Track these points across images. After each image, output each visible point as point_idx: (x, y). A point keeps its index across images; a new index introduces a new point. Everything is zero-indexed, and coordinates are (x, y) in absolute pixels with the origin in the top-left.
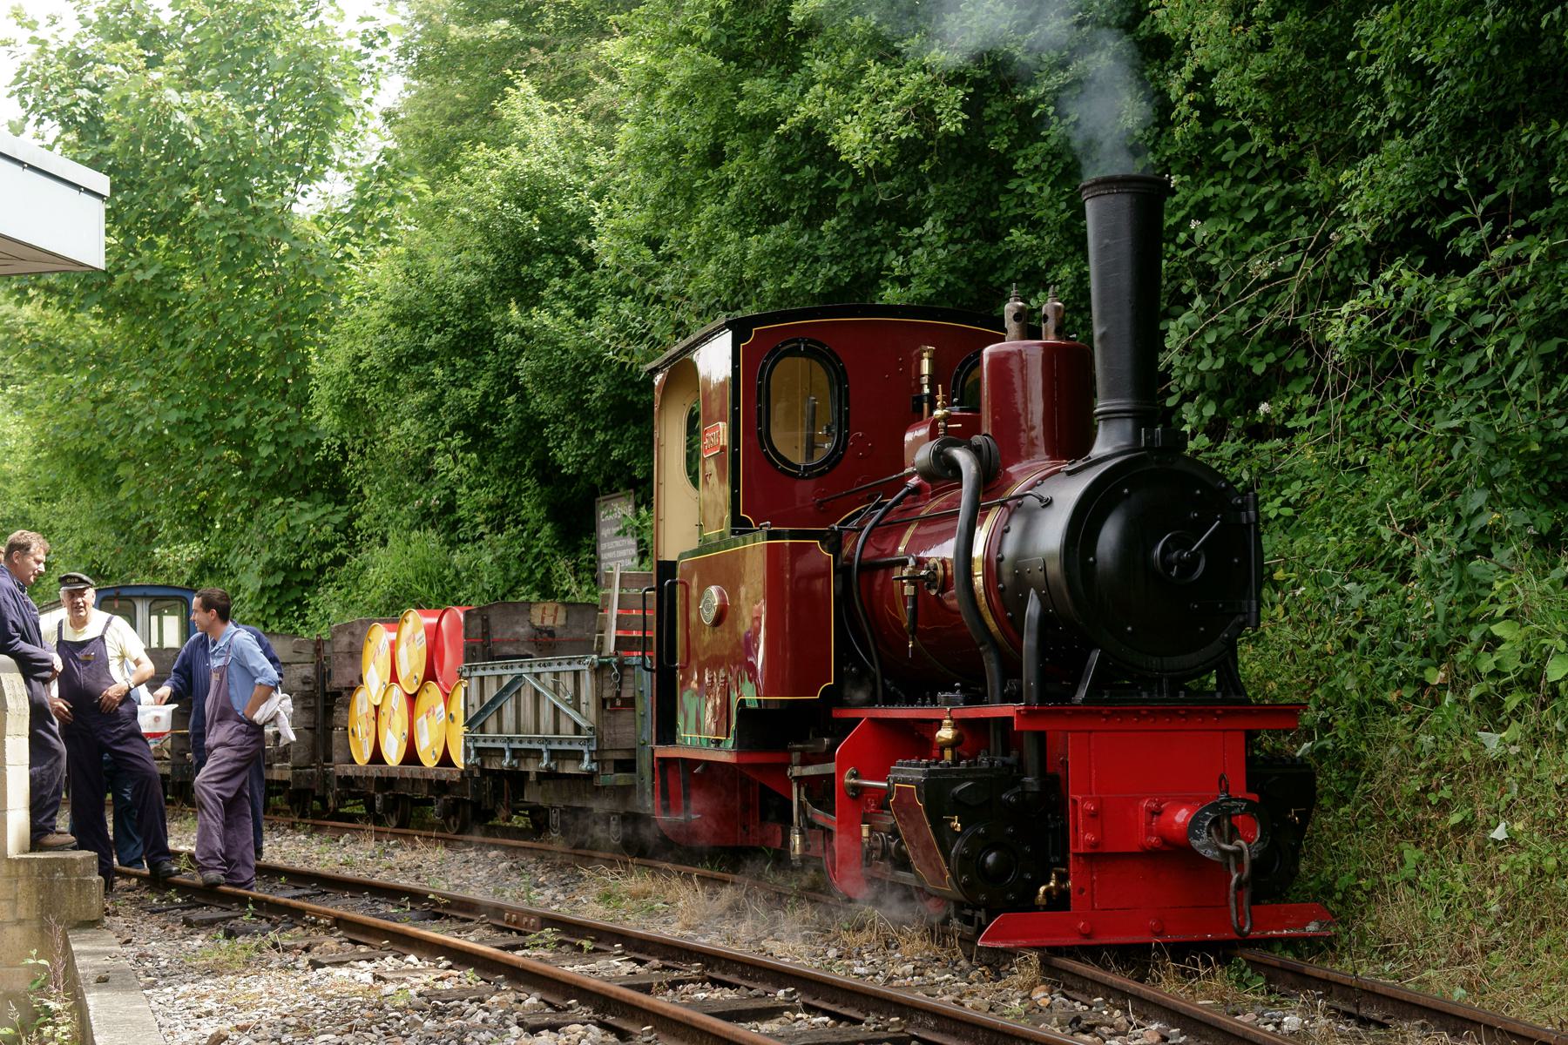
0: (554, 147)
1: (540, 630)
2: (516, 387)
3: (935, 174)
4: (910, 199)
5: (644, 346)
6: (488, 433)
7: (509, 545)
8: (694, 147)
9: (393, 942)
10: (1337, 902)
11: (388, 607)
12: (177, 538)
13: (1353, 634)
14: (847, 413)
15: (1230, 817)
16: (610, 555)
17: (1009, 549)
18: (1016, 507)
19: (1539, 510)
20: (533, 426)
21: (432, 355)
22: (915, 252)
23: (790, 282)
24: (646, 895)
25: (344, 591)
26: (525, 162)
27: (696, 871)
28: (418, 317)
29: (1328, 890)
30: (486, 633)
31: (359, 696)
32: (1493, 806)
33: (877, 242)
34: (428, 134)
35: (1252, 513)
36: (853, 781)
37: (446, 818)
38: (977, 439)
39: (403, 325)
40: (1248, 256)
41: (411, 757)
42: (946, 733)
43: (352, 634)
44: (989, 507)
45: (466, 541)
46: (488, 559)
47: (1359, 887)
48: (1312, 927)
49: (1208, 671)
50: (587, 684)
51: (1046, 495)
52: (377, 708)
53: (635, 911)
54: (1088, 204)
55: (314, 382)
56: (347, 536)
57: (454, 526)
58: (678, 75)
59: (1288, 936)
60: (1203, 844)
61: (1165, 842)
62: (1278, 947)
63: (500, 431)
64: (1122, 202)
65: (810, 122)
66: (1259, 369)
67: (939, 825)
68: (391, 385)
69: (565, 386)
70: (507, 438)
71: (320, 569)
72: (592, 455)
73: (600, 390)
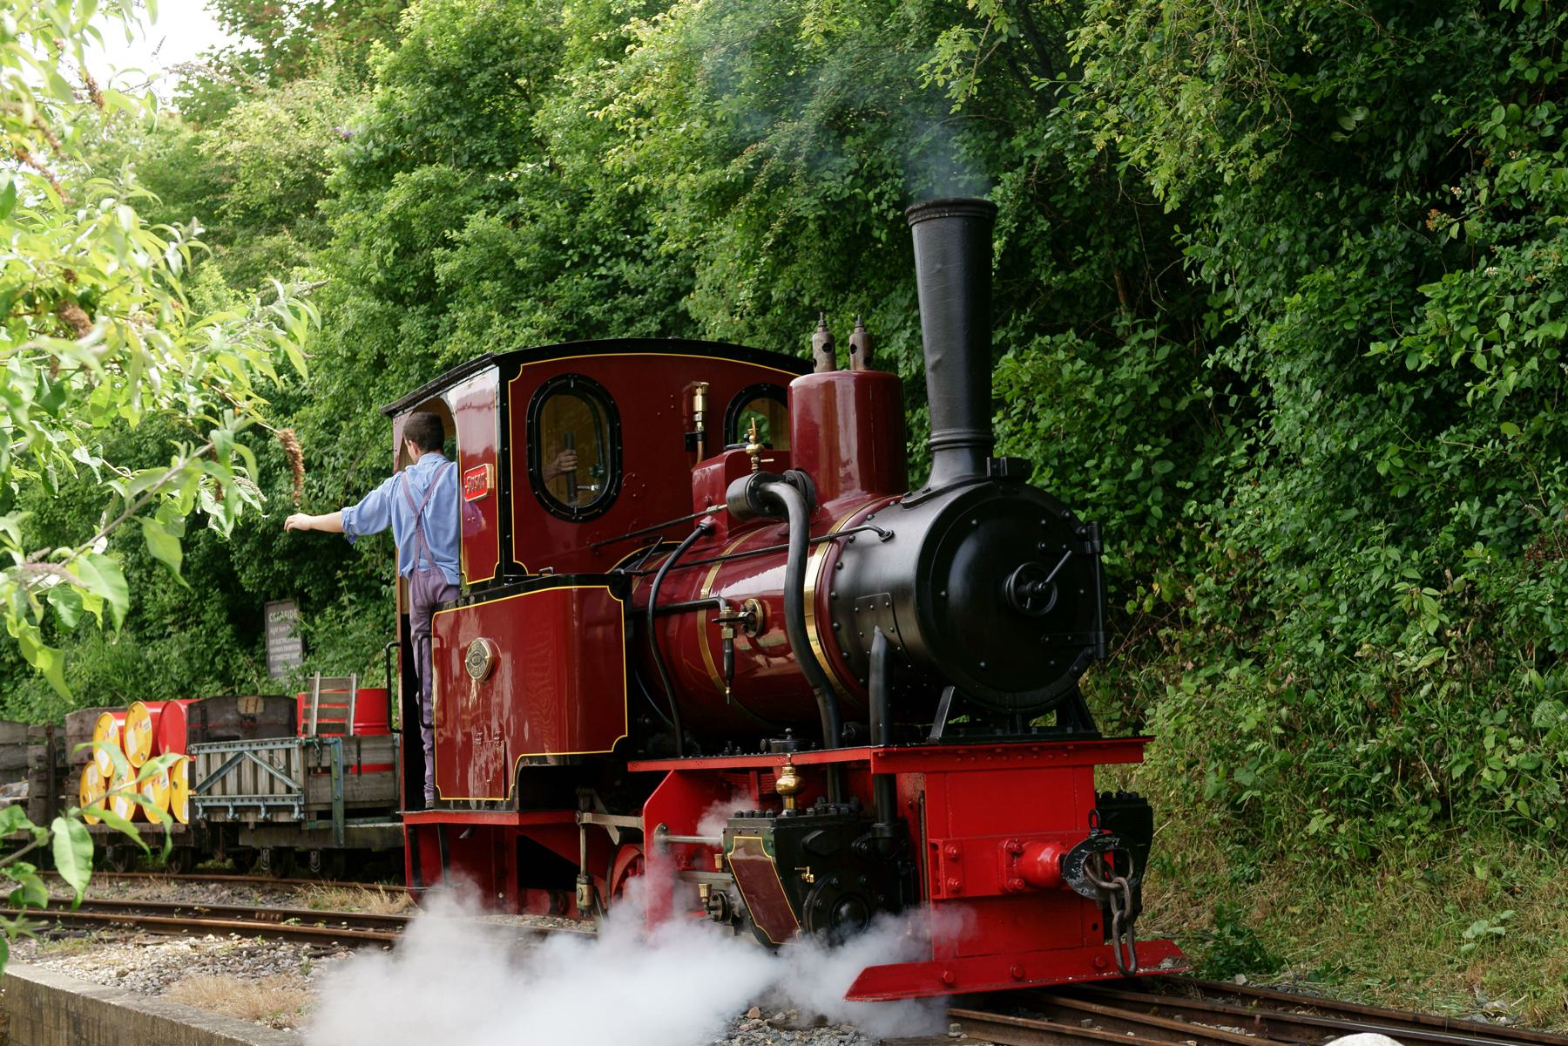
1: (245, 717)
30: (204, 720)
38: (791, 473)
44: (815, 545)
49: (1049, 710)
50: (296, 758)
51: (886, 528)
52: (107, 780)
54: (915, 230)
60: (1081, 882)
61: (1027, 883)
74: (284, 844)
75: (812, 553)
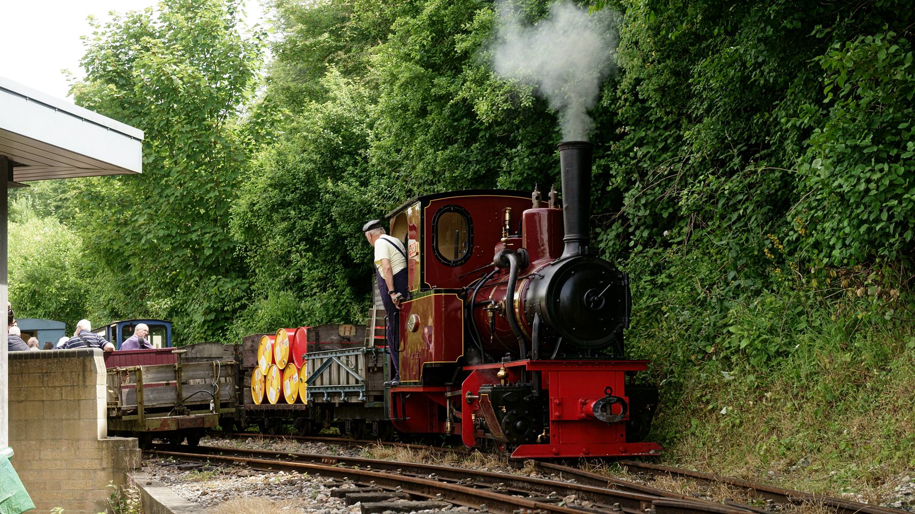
0: (349, 102)
1: (343, 338)
4: (512, 135)
5: (391, 202)
6: (317, 243)
7: (329, 298)
8: (412, 109)
10: (667, 443)
11: (268, 329)
12: (158, 296)
14: (472, 237)
20: (339, 239)
21: (290, 204)
23: (457, 173)
25: (246, 322)
26: (334, 110)
28: (283, 185)
30: (317, 339)
31: (256, 371)
33: (498, 154)
38: (520, 250)
39: (275, 188)
41: (282, 399)
42: (501, 373)
43: (253, 341)
44: (522, 279)
45: (307, 296)
46: (318, 305)
47: (676, 437)
52: (265, 377)
56: (247, 293)
57: (301, 289)
58: (404, 77)
63: (323, 242)
65: (464, 100)
66: (665, 215)
67: (497, 410)
68: (269, 218)
69: (355, 220)
70: (327, 245)
71: (234, 311)
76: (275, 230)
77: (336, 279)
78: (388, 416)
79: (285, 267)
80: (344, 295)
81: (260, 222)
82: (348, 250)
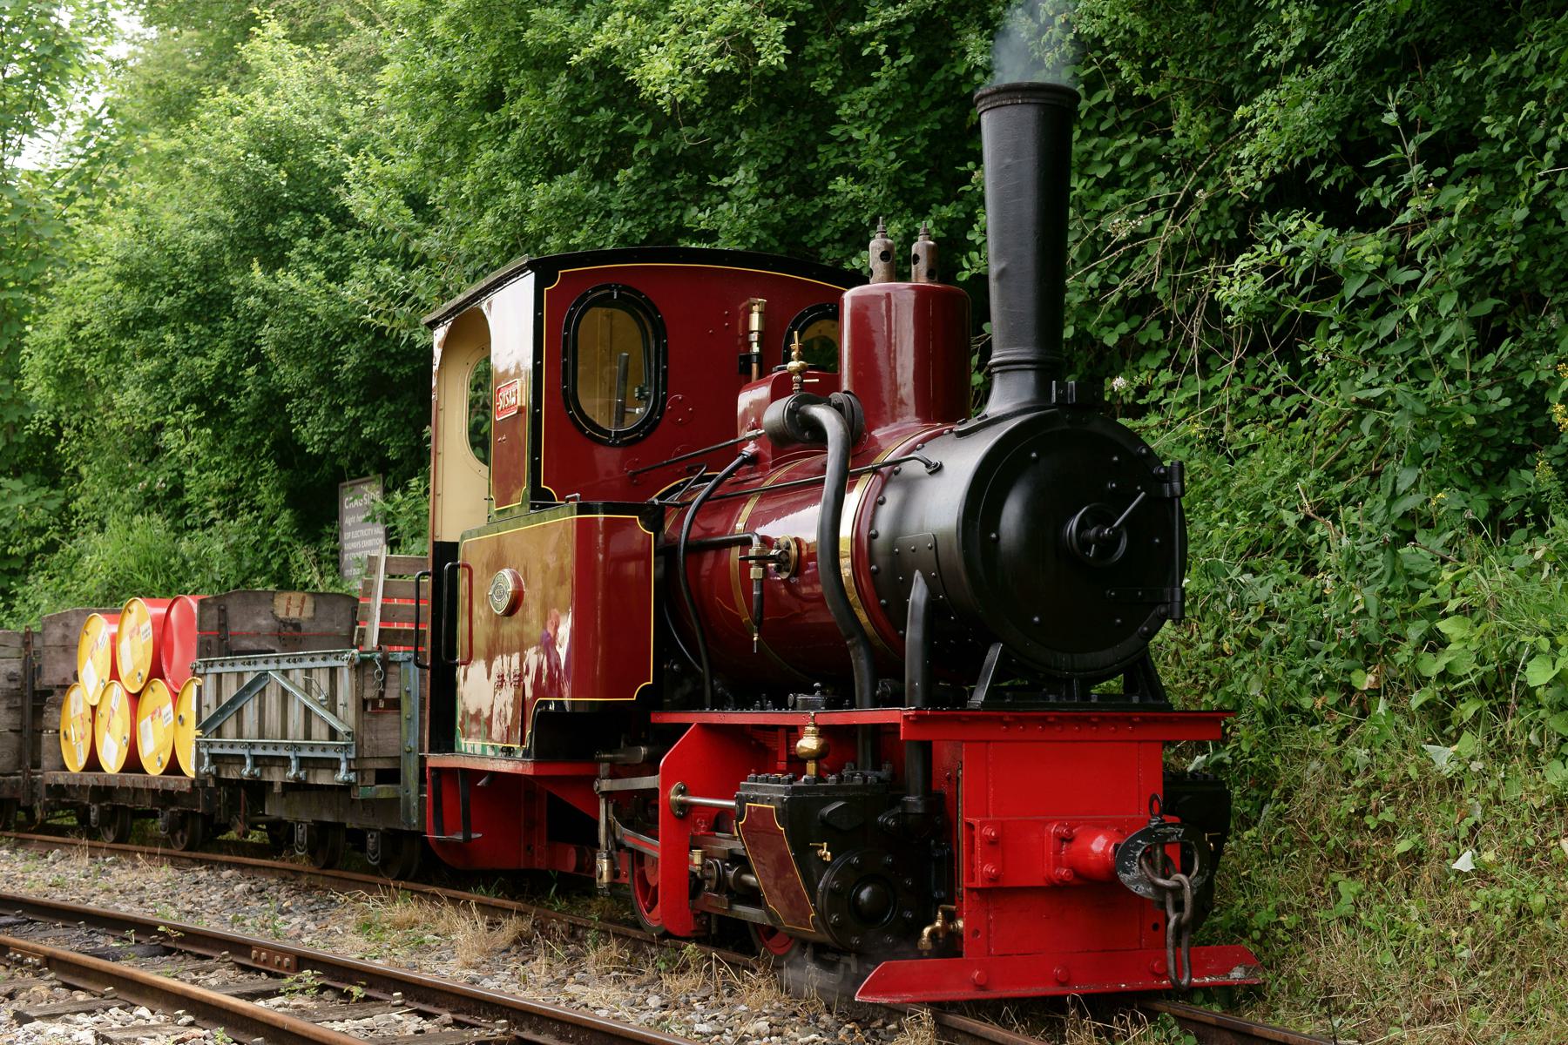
1: (284, 623)
2: (257, 357)
3: (745, 120)
4: (716, 148)
5: (406, 309)
8: (470, 86)
9: (118, 988)
10: (1254, 941)
11: (106, 598)
13: (1255, 632)
15: (1163, 846)
16: (354, 545)
17: (883, 526)
18: (890, 474)
19: (1473, 493)
20: (274, 401)
21: (164, 319)
22: (720, 207)
24: (413, 924)
26: (273, 109)
27: (473, 897)
28: (147, 277)
29: (1242, 929)
30: (223, 625)
31: (74, 695)
32: (1451, 832)
34: (161, 85)
35: (1176, 485)
36: (680, 797)
37: (172, 833)
38: (836, 397)
39: (130, 285)
40: (1101, 214)
41: (133, 763)
42: (809, 743)
43: (66, 626)
44: (858, 475)
45: (192, 528)
46: (219, 547)
47: (1280, 924)
48: (1237, 974)
50: (345, 682)
51: (934, 460)
52: (94, 709)
53: (403, 944)
54: (985, 118)
55: (26, 350)
56: (62, 521)
57: (181, 512)
59: (1212, 985)
60: (1135, 879)
61: (1077, 873)
62: (1199, 998)
64: (1027, 115)
65: (609, 51)
66: (1111, 339)
68: (114, 355)
71: (30, 558)
72: (341, 433)
73: (352, 360)
74: (328, 818)
75: (853, 485)
76: (129, 376)
77: (259, 492)
78: (408, 818)
79: (146, 463)
80: (276, 527)
81: (90, 365)
82: (294, 426)
